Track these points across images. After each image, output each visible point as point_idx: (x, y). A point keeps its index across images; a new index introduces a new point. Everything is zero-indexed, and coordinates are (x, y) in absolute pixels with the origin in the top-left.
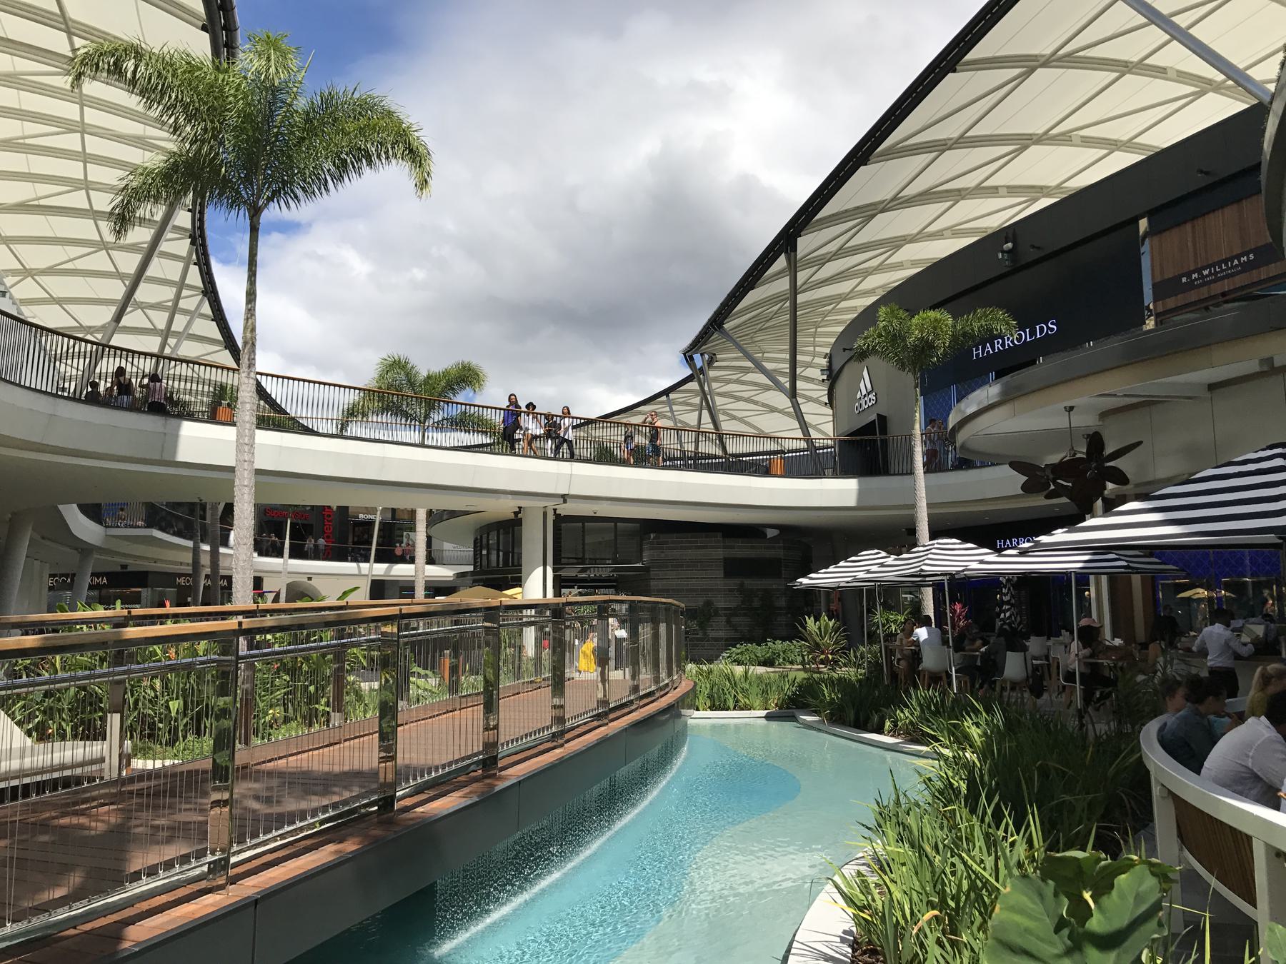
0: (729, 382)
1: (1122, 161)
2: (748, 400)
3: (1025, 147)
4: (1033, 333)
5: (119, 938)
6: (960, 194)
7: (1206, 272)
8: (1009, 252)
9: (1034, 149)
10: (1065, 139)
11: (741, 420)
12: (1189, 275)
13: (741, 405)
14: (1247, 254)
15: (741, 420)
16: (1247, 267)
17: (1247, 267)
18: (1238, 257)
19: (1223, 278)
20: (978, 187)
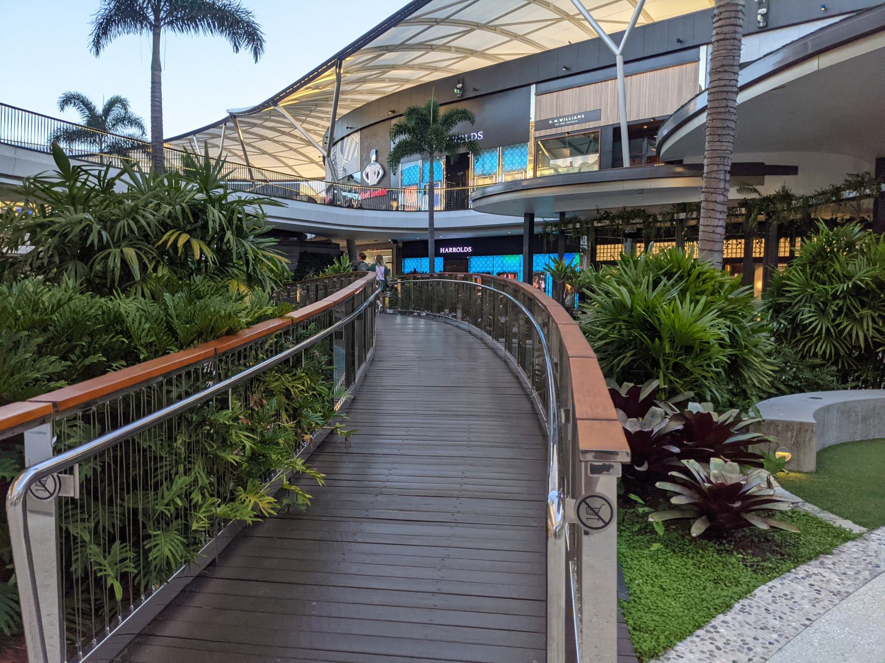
0: (284, 133)
1: (528, 50)
2: (295, 150)
3: (472, 30)
4: (188, 245)
5: (743, 279)
6: (432, 48)
7: (556, 121)
8: (460, 89)
9: (478, 32)
10: (494, 29)
11: (290, 167)
12: (553, 119)
13: (292, 154)
14: (580, 114)
15: (290, 167)
16: (580, 121)
17: (580, 121)
18: (577, 115)
19: (568, 125)
20: (444, 45)
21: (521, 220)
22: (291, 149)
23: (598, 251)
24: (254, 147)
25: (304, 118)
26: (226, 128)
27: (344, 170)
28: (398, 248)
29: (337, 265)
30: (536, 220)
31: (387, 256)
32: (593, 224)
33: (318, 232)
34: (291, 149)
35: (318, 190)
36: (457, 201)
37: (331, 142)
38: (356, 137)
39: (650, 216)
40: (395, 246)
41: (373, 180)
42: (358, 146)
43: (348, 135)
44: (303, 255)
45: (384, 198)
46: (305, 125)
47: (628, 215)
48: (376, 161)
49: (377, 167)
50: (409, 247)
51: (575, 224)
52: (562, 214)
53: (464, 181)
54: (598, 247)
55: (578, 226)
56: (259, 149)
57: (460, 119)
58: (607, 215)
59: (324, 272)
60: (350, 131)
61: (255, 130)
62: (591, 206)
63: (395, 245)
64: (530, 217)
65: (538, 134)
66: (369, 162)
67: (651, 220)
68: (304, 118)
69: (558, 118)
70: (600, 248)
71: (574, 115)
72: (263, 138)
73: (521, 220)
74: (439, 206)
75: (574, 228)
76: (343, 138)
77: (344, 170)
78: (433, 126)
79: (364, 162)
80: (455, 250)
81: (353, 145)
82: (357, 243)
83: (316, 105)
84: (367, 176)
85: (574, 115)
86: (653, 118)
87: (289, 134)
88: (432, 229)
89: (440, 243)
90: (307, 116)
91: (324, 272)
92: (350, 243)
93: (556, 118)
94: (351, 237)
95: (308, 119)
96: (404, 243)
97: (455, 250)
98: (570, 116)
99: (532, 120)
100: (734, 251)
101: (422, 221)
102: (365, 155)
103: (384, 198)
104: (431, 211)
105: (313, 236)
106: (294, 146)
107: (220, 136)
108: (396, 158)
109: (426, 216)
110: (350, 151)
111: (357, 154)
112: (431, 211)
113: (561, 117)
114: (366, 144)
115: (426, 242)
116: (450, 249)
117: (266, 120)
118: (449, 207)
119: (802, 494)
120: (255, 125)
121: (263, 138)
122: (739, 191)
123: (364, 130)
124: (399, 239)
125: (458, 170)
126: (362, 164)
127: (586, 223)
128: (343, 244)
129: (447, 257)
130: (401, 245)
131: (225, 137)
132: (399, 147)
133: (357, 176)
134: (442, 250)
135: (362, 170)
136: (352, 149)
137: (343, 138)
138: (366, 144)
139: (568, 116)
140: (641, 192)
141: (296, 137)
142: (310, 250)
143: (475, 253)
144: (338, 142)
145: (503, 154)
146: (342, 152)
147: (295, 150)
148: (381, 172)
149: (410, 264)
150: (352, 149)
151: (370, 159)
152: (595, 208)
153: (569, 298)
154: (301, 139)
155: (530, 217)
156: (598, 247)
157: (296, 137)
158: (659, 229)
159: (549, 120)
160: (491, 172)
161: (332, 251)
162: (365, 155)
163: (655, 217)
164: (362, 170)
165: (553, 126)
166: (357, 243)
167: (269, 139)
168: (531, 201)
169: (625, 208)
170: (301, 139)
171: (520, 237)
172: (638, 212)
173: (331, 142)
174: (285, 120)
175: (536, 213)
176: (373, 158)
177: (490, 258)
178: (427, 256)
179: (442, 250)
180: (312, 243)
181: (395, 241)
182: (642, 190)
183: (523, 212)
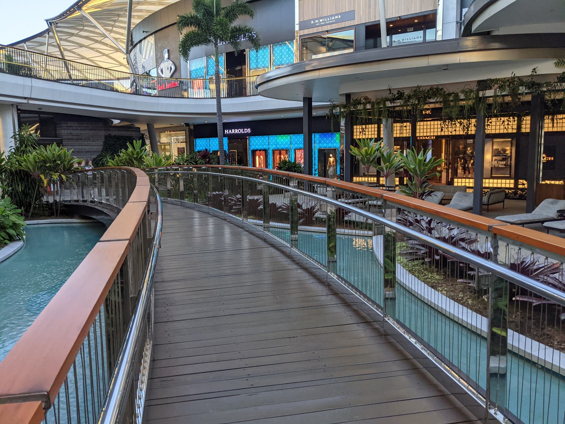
0: (97, 41)
2: (107, 55)
7: (317, 21)
12: (314, 20)
18: (334, 15)
21: (300, 104)
22: (104, 54)
23: (355, 130)
24: (74, 53)
25: (110, 28)
26: (49, 37)
27: (143, 67)
28: (190, 130)
29: (130, 149)
30: (314, 104)
31: (182, 136)
32: (384, 104)
33: (123, 118)
34: (104, 54)
35: (125, 86)
36: (237, 90)
37: (131, 45)
38: (151, 39)
39: (450, 94)
40: (187, 128)
41: (167, 74)
42: (153, 46)
43: (145, 38)
44: (107, 138)
45: (176, 87)
46: (113, 35)
47: (422, 95)
48: (169, 58)
49: (170, 64)
50: (199, 129)
51: (365, 104)
52: (348, 96)
53: (241, 73)
54: (355, 127)
55: (368, 106)
56: (78, 55)
57: (242, 13)
58: (400, 95)
59: (119, 156)
60: (146, 34)
61: (73, 39)
62: (383, 86)
63: (187, 127)
64: (308, 101)
65: (302, 33)
66: (163, 59)
67: (451, 98)
68: (110, 28)
69: (318, 19)
70: (357, 129)
71: (332, 16)
72: (81, 46)
73: (300, 104)
74: (223, 93)
75: (365, 109)
76: (140, 41)
77: (143, 67)
78: (216, 19)
79: (159, 60)
80: (237, 131)
81: (149, 46)
82: (156, 126)
83: (119, 15)
84: (162, 71)
85: (332, 16)
86: (400, 17)
87: (100, 42)
88: (220, 114)
89: (227, 126)
90: (113, 26)
91: (119, 156)
92: (150, 127)
93: (316, 19)
94: (151, 122)
95: (114, 29)
96: (195, 126)
97: (237, 131)
98: (329, 16)
99: (297, 21)
100: (425, 127)
101: (211, 106)
102: (159, 54)
103: (176, 87)
104: (219, 98)
105: (119, 121)
106: (106, 52)
107: (44, 44)
108: (185, 49)
109: (214, 102)
110: (147, 51)
111: (153, 53)
112: (219, 98)
113: (321, 18)
114: (160, 45)
115: (215, 125)
116: (233, 130)
117: (81, 30)
118: (231, 94)
119: (546, 341)
120: (72, 35)
121: (81, 46)
122: (557, 64)
123: (158, 34)
124: (191, 122)
125: (236, 62)
126: (157, 62)
127: (378, 103)
128: (143, 128)
129: (231, 137)
130: (192, 127)
131: (49, 45)
132: (187, 36)
133: (154, 73)
134: (226, 132)
135: (157, 66)
136: (149, 49)
137: (140, 41)
138: (160, 45)
139: (326, 17)
140: (446, 68)
141: (106, 45)
142: (114, 133)
143: (254, 134)
144: (137, 44)
145: (273, 50)
146: (141, 53)
147: (107, 55)
148: (173, 68)
149: (201, 144)
150: (149, 49)
151: (163, 57)
152: (386, 87)
153: (331, 169)
154: (111, 47)
155: (308, 101)
156: (355, 127)
157: (106, 45)
158: (462, 107)
159: (311, 20)
160: (263, 64)
161: (134, 134)
162: (159, 54)
163: (456, 95)
164: (157, 66)
165: (314, 26)
166: (156, 126)
167: (86, 47)
168: (309, 85)
169: (419, 87)
170: (111, 47)
171: (301, 119)
172: (435, 91)
173: (131, 45)
174: (97, 30)
175: (314, 97)
176: (166, 56)
177: (266, 138)
178: (217, 137)
179: (226, 132)
180: (116, 127)
181: (187, 125)
182: (447, 65)
183: (301, 97)
